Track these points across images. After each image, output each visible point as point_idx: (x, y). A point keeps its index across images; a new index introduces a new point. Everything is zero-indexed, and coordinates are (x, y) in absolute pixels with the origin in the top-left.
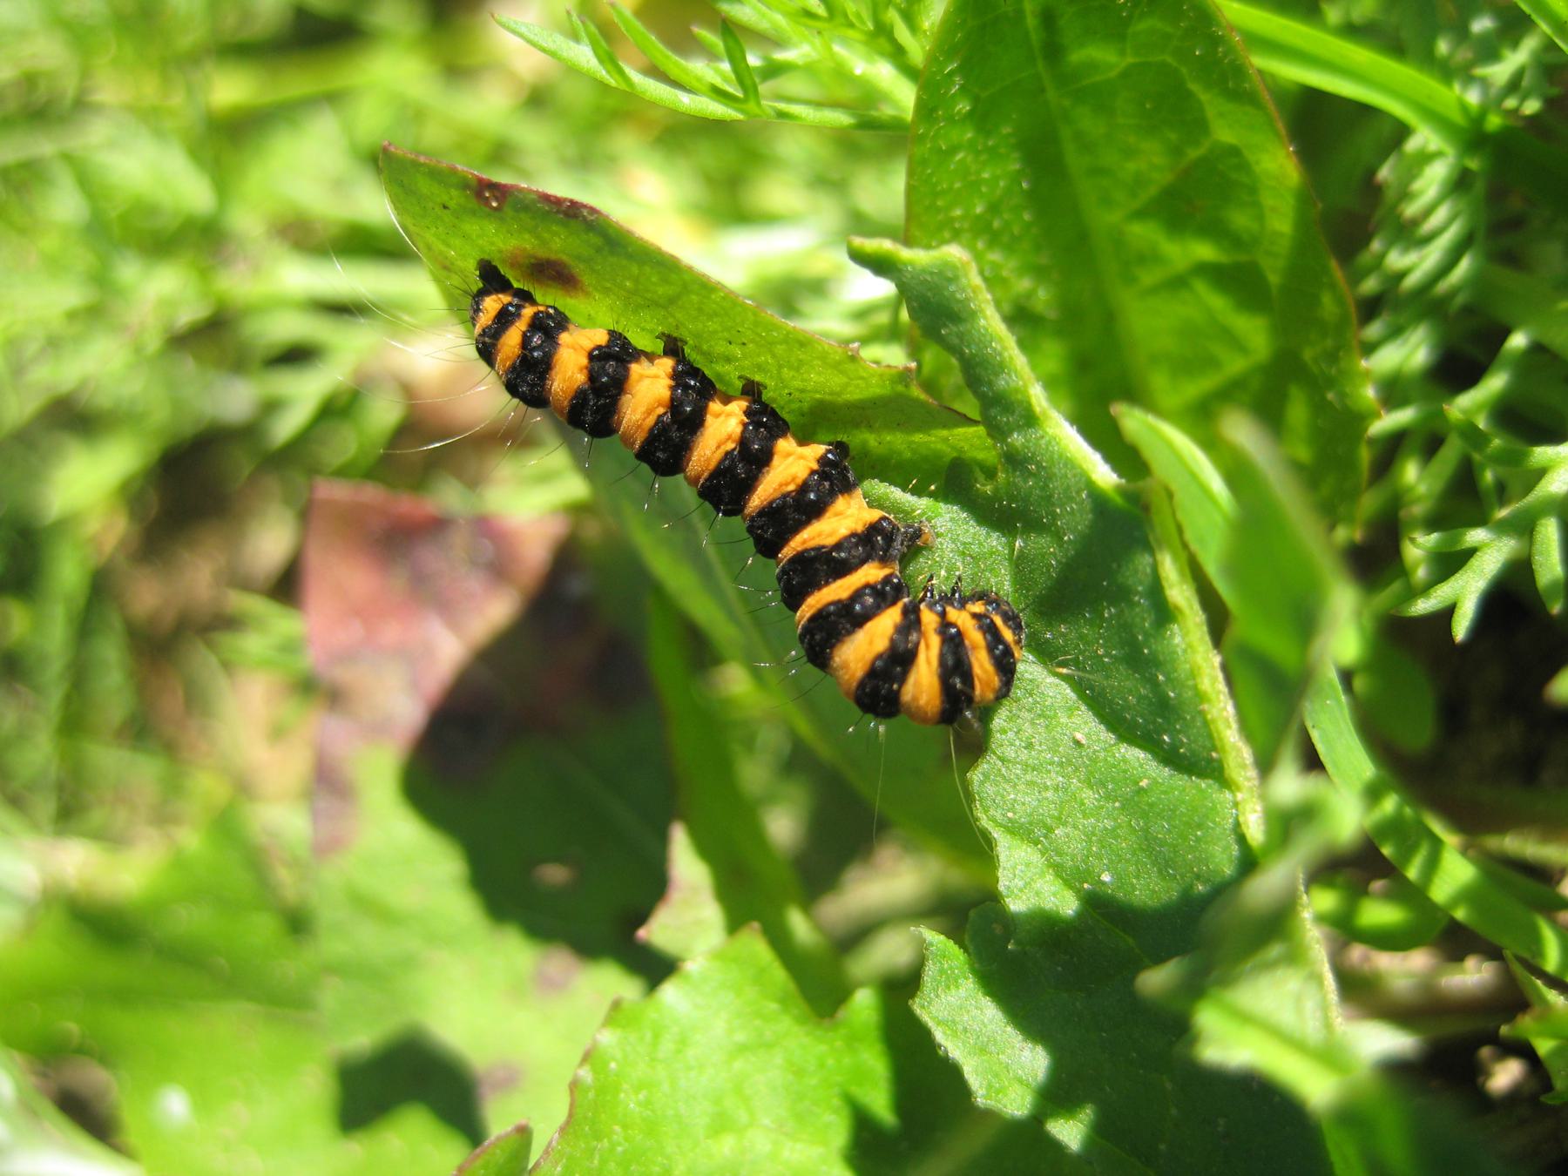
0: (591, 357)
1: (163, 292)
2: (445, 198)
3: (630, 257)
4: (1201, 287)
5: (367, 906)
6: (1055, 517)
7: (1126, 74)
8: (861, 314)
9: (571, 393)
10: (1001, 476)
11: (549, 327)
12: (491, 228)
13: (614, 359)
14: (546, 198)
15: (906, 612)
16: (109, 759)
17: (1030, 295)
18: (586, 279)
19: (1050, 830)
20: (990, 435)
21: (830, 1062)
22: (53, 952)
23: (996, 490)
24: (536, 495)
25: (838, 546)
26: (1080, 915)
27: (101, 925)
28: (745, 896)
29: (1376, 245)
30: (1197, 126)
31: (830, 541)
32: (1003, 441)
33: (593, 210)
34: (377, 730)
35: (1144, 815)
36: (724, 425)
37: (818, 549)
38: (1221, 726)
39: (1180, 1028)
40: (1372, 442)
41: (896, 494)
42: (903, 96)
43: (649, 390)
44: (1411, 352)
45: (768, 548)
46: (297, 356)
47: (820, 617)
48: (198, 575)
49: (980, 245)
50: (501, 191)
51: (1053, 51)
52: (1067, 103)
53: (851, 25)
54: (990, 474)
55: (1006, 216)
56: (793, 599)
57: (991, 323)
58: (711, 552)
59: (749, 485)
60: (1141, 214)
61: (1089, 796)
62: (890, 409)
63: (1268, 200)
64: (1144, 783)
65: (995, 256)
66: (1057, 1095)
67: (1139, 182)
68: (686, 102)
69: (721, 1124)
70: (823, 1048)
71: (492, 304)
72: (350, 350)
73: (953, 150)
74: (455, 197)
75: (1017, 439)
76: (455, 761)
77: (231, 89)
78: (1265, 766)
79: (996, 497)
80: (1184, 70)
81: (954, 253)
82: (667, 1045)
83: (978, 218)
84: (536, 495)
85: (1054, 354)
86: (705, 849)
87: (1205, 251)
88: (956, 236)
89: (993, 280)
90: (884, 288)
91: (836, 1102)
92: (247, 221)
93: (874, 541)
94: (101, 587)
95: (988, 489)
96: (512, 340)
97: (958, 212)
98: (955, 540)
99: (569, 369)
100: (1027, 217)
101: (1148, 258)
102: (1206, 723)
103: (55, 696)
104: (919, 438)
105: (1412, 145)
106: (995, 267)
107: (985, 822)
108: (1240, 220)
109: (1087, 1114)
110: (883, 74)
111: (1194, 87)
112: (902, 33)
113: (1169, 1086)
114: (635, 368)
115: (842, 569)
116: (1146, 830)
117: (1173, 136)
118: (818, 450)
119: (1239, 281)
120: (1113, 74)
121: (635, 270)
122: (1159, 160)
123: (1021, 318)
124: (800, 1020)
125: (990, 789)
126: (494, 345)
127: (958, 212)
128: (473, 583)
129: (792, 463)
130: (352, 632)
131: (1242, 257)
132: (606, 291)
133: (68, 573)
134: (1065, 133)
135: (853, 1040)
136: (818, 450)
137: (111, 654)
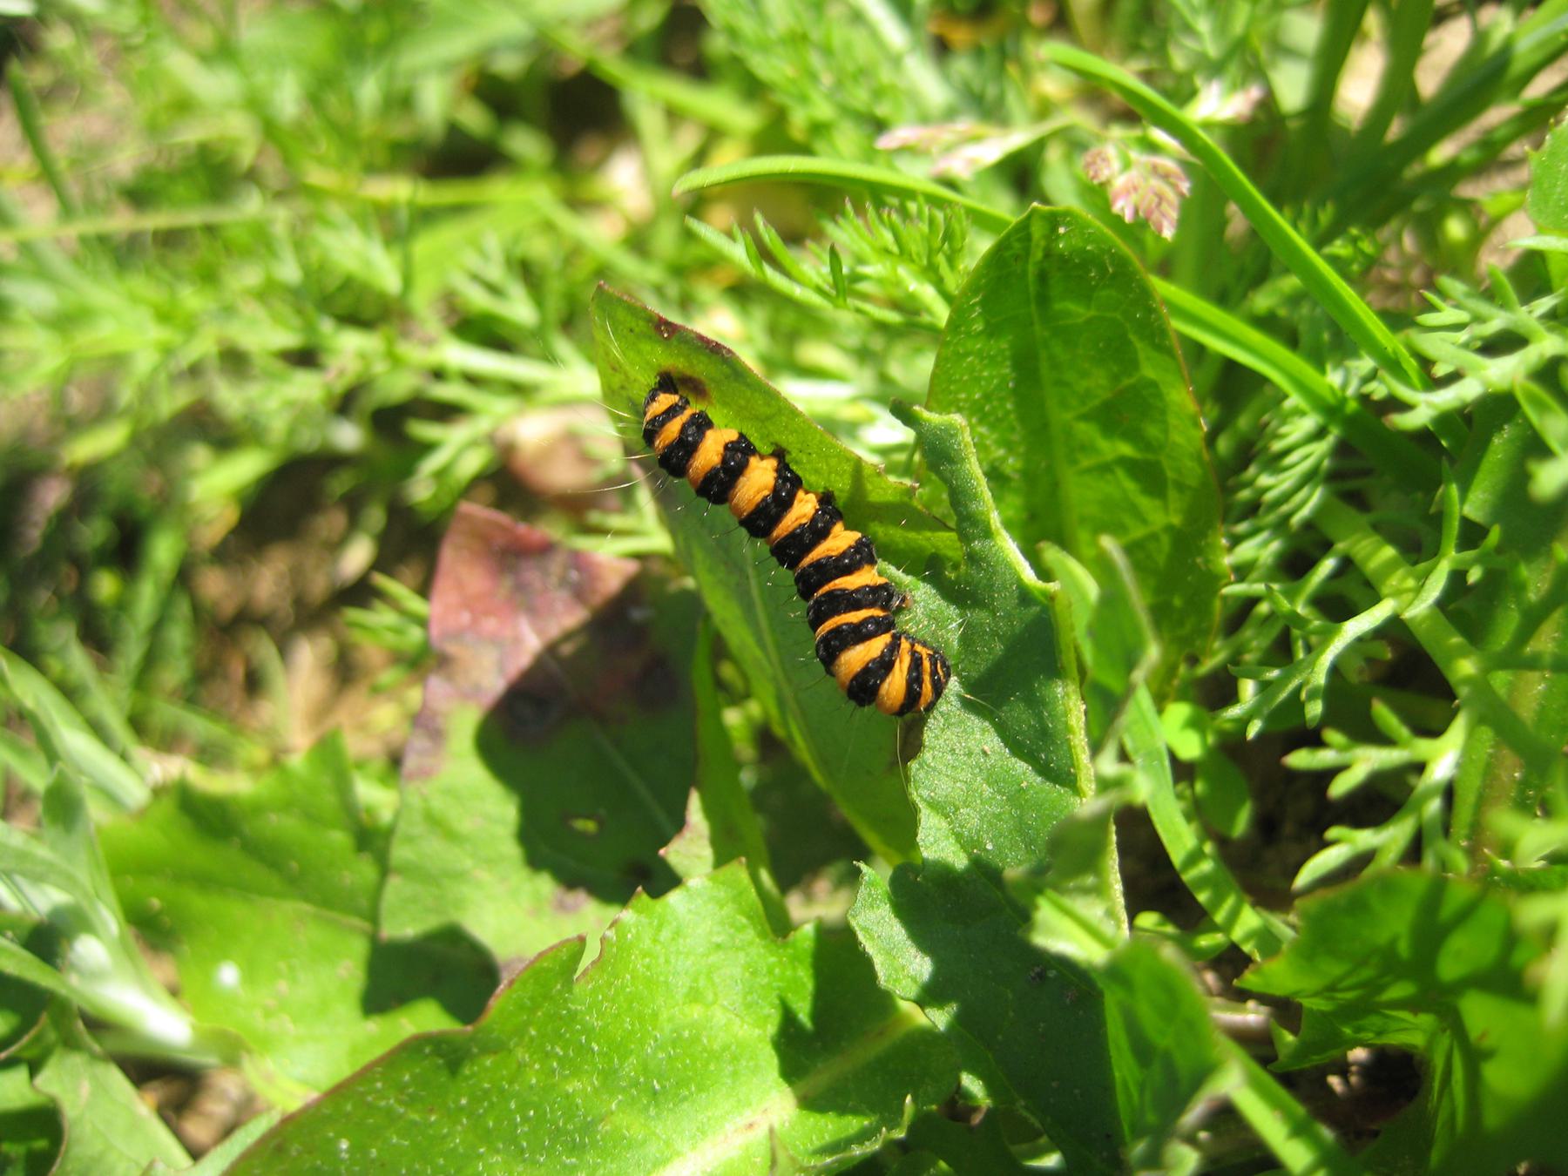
0: (726, 447)
1: (350, 349)
2: (633, 325)
3: (748, 385)
4: (1121, 474)
5: (435, 823)
6: (993, 599)
7: (1089, 321)
8: (884, 452)
9: (707, 469)
10: (963, 568)
11: (702, 424)
12: (659, 350)
13: (739, 454)
14: (701, 338)
15: (894, 636)
16: (166, 712)
17: (1003, 460)
18: (714, 394)
19: (957, 809)
20: (960, 539)
21: (777, 971)
22: (161, 836)
23: (958, 577)
24: (639, 533)
25: (857, 591)
26: (968, 870)
27: (206, 817)
28: (726, 847)
29: (1252, 470)
30: (1132, 364)
31: (852, 587)
32: (968, 545)
33: (729, 351)
34: (467, 696)
35: (1021, 807)
36: (804, 507)
37: (843, 590)
38: (1079, 750)
39: (1025, 917)
40: (1225, 598)
41: (892, 570)
42: (941, 313)
43: (759, 478)
44: (1261, 549)
45: (806, 594)
46: (447, 412)
47: (837, 631)
48: (268, 581)
49: (974, 421)
50: (673, 328)
51: (1043, 300)
52: (1046, 334)
53: (912, 261)
54: (956, 567)
55: (995, 403)
56: (815, 624)
57: (974, 469)
58: (755, 592)
59: (777, 519)
60: (1085, 417)
61: (987, 791)
62: (899, 512)
63: (1172, 420)
64: (1024, 785)
65: (982, 430)
66: (930, 995)
67: (1086, 396)
68: (797, 292)
69: (694, 995)
70: (772, 959)
71: (665, 400)
72: (493, 413)
73: (967, 354)
74: (641, 326)
75: (977, 545)
76: (521, 728)
77: (401, 190)
78: (1096, 749)
79: (957, 582)
80: (1128, 325)
81: (957, 419)
82: (665, 934)
83: (975, 402)
84: (639, 533)
85: (1014, 501)
86: (709, 811)
87: (1126, 449)
88: (959, 410)
89: (980, 446)
90: (905, 435)
91: (777, 1002)
92: (423, 302)
93: (881, 595)
94: (184, 577)
95: (953, 576)
96: (673, 428)
97: (963, 396)
98: (926, 610)
99: (710, 453)
100: (1009, 406)
101: (1087, 448)
102: (1070, 748)
103: (131, 652)
104: (912, 535)
105: (1288, 404)
106: (981, 436)
107: (915, 797)
108: (1152, 431)
109: (953, 1008)
110: (927, 293)
111: (1132, 337)
112: (944, 269)
113: (1010, 996)
114: (754, 461)
115: (857, 606)
116: (1020, 818)
117: (1115, 369)
118: (857, 535)
119: (1149, 476)
120: (1080, 320)
121: (749, 393)
122: (1103, 382)
123: (995, 475)
124: (762, 935)
125: (922, 774)
126: (663, 424)
127: (963, 396)
128: (561, 597)
129: (841, 539)
130: (465, 618)
131: (1150, 456)
132: (725, 404)
133: (163, 551)
134: (1043, 354)
135: (795, 959)
136: (857, 535)
137: (178, 636)
